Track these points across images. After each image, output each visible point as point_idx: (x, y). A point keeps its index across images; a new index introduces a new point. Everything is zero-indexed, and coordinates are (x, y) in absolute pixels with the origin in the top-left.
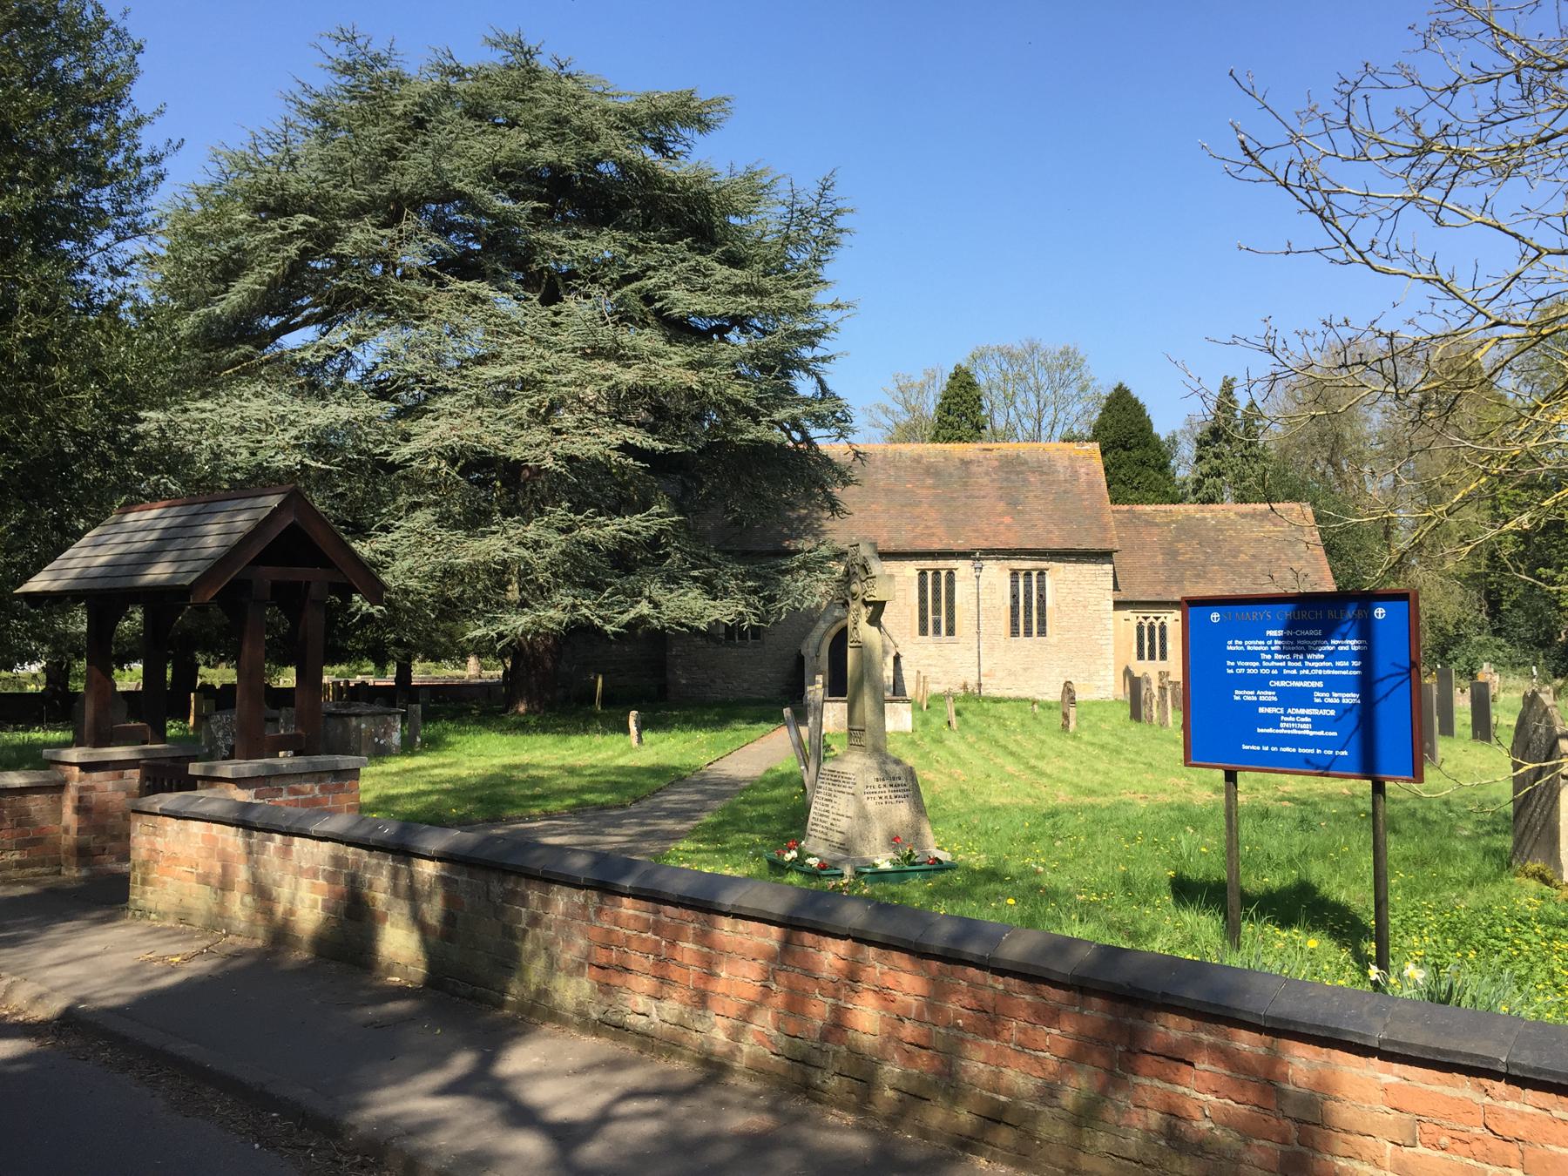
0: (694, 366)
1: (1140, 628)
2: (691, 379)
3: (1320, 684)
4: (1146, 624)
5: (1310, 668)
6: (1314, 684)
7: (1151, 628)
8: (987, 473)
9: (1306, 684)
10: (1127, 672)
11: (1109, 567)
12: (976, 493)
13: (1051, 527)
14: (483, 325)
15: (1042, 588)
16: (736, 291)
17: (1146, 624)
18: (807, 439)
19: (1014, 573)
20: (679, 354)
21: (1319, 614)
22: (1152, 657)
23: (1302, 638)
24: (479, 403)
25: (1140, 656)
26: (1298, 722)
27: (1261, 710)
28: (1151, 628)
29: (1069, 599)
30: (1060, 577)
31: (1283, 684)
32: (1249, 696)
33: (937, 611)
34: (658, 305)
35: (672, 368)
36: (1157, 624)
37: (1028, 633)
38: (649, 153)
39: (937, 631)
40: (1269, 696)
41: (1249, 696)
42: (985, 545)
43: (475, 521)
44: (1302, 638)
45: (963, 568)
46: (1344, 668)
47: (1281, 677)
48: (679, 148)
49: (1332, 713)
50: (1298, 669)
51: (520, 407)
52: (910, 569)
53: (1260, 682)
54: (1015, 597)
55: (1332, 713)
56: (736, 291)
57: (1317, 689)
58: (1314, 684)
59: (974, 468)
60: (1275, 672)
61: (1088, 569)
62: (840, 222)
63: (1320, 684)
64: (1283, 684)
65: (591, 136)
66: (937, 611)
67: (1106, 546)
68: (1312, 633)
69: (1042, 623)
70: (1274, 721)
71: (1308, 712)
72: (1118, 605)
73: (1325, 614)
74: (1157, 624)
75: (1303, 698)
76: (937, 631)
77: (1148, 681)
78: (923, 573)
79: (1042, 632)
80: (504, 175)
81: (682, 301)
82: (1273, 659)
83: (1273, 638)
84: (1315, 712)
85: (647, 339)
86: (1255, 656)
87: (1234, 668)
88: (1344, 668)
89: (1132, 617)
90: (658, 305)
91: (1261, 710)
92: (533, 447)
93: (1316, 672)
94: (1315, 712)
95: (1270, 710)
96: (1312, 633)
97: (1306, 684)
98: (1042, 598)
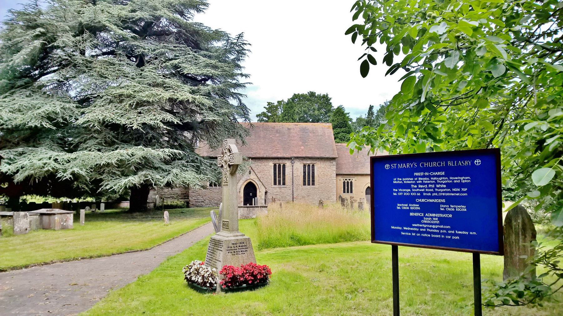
0: (193, 92)
1: (344, 183)
2: (190, 97)
3: (444, 201)
4: (346, 181)
5: (438, 192)
6: (440, 201)
7: (348, 183)
8: (296, 133)
9: (436, 201)
10: (340, 197)
11: (334, 163)
12: (293, 139)
13: (316, 150)
14: (127, 80)
15: (313, 170)
16: (207, 66)
17: (346, 181)
18: (235, 119)
19: (305, 166)
20: (187, 87)
21: (443, 164)
22: (348, 192)
23: (434, 176)
24: (111, 102)
25: (344, 192)
26: (431, 220)
27: (411, 214)
28: (348, 183)
29: (322, 173)
30: (319, 167)
31: (423, 200)
32: (405, 207)
33: (279, 177)
34: (179, 70)
35: (184, 93)
36: (350, 181)
37: (309, 184)
38: (179, 16)
39: (279, 184)
40: (416, 207)
41: (405, 207)
42: (295, 155)
43: (110, 144)
44: (434, 176)
45: (288, 163)
46: (457, 192)
47: (422, 197)
48: (189, 16)
49: (450, 216)
50: (431, 193)
51: (126, 104)
52: (271, 164)
53: (410, 200)
54: (304, 172)
55: (450, 216)
56: (207, 66)
57: (442, 203)
58: (440, 201)
59: (292, 131)
60: (419, 194)
61: (328, 163)
62: (246, 47)
63: (444, 201)
64: (423, 200)
65: (155, 9)
66: (279, 177)
67: (334, 156)
68: (439, 173)
69: (313, 181)
70: (418, 220)
71: (437, 215)
72: (337, 175)
73: (446, 163)
74: (350, 181)
75: (435, 208)
76: (279, 184)
77: (347, 200)
78: (275, 165)
79: (313, 184)
80: (125, 23)
81: (190, 70)
82: (418, 188)
83: (418, 177)
84: (441, 215)
85: (174, 82)
86: (408, 186)
87: (397, 192)
88: (457, 192)
89: (342, 180)
90: (179, 70)
91: (411, 214)
92: (134, 121)
93: (441, 194)
94: (441, 215)
95: (416, 214)
96: (439, 173)
97: (436, 201)
98: (313, 173)
